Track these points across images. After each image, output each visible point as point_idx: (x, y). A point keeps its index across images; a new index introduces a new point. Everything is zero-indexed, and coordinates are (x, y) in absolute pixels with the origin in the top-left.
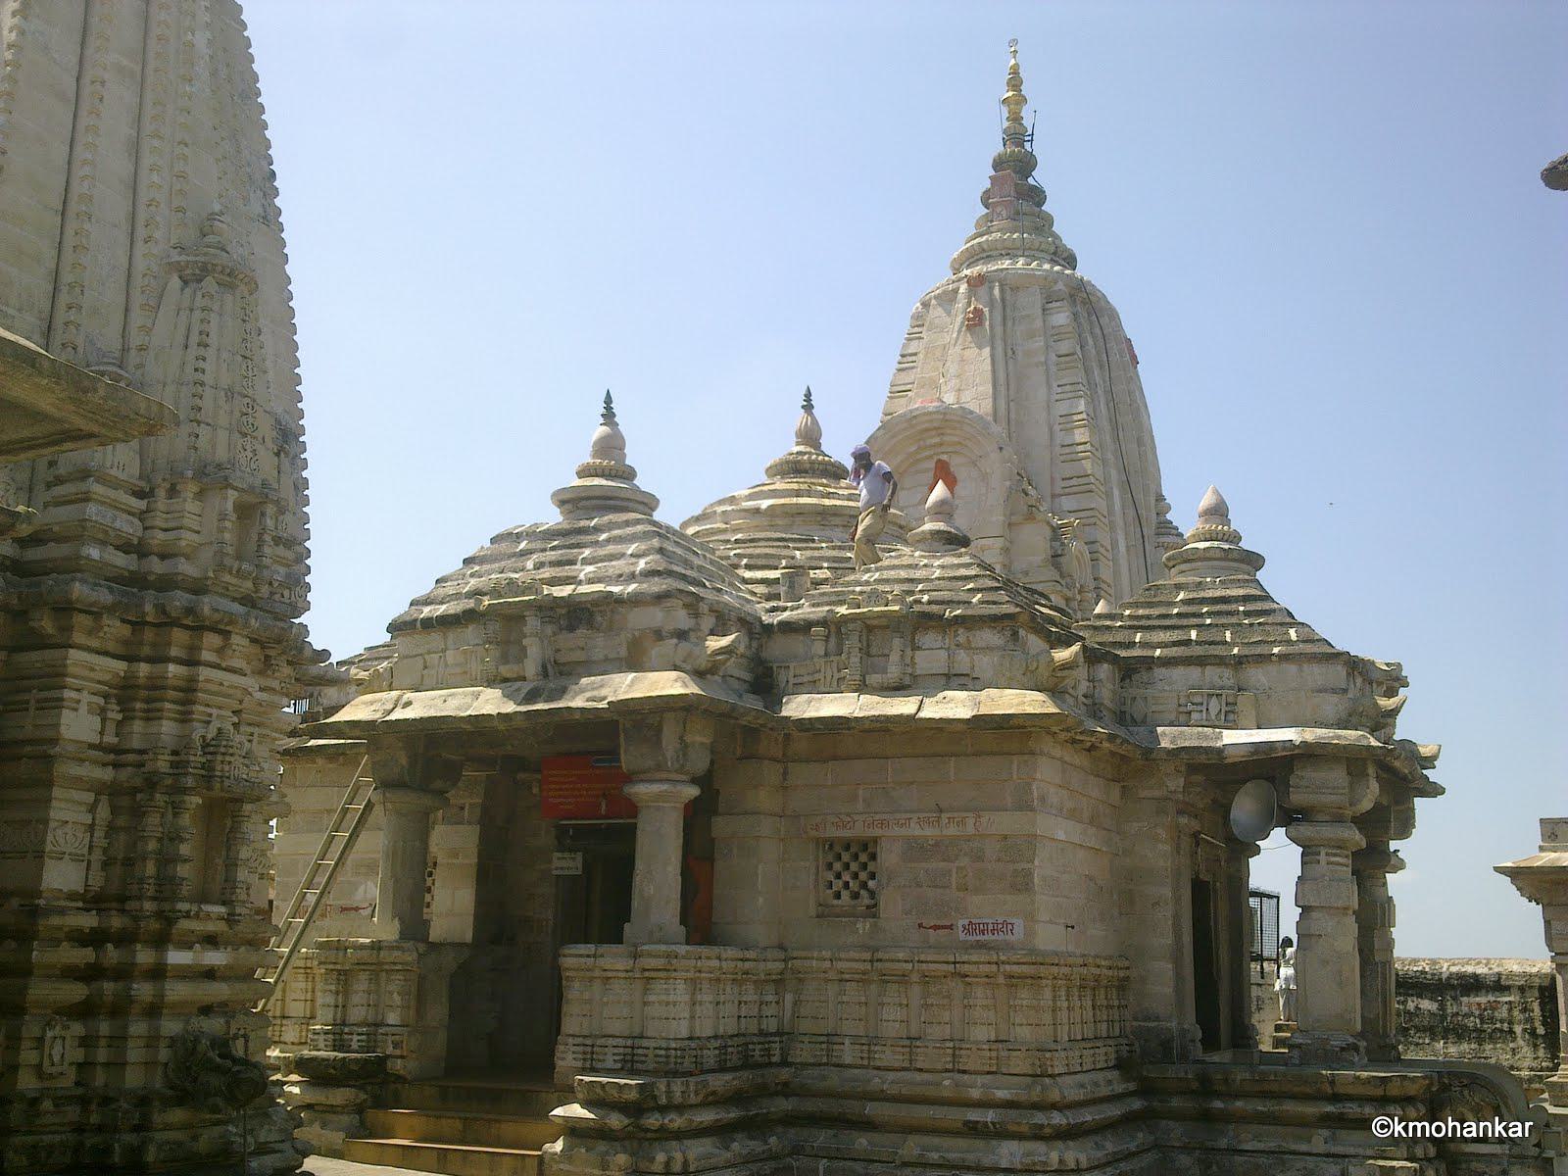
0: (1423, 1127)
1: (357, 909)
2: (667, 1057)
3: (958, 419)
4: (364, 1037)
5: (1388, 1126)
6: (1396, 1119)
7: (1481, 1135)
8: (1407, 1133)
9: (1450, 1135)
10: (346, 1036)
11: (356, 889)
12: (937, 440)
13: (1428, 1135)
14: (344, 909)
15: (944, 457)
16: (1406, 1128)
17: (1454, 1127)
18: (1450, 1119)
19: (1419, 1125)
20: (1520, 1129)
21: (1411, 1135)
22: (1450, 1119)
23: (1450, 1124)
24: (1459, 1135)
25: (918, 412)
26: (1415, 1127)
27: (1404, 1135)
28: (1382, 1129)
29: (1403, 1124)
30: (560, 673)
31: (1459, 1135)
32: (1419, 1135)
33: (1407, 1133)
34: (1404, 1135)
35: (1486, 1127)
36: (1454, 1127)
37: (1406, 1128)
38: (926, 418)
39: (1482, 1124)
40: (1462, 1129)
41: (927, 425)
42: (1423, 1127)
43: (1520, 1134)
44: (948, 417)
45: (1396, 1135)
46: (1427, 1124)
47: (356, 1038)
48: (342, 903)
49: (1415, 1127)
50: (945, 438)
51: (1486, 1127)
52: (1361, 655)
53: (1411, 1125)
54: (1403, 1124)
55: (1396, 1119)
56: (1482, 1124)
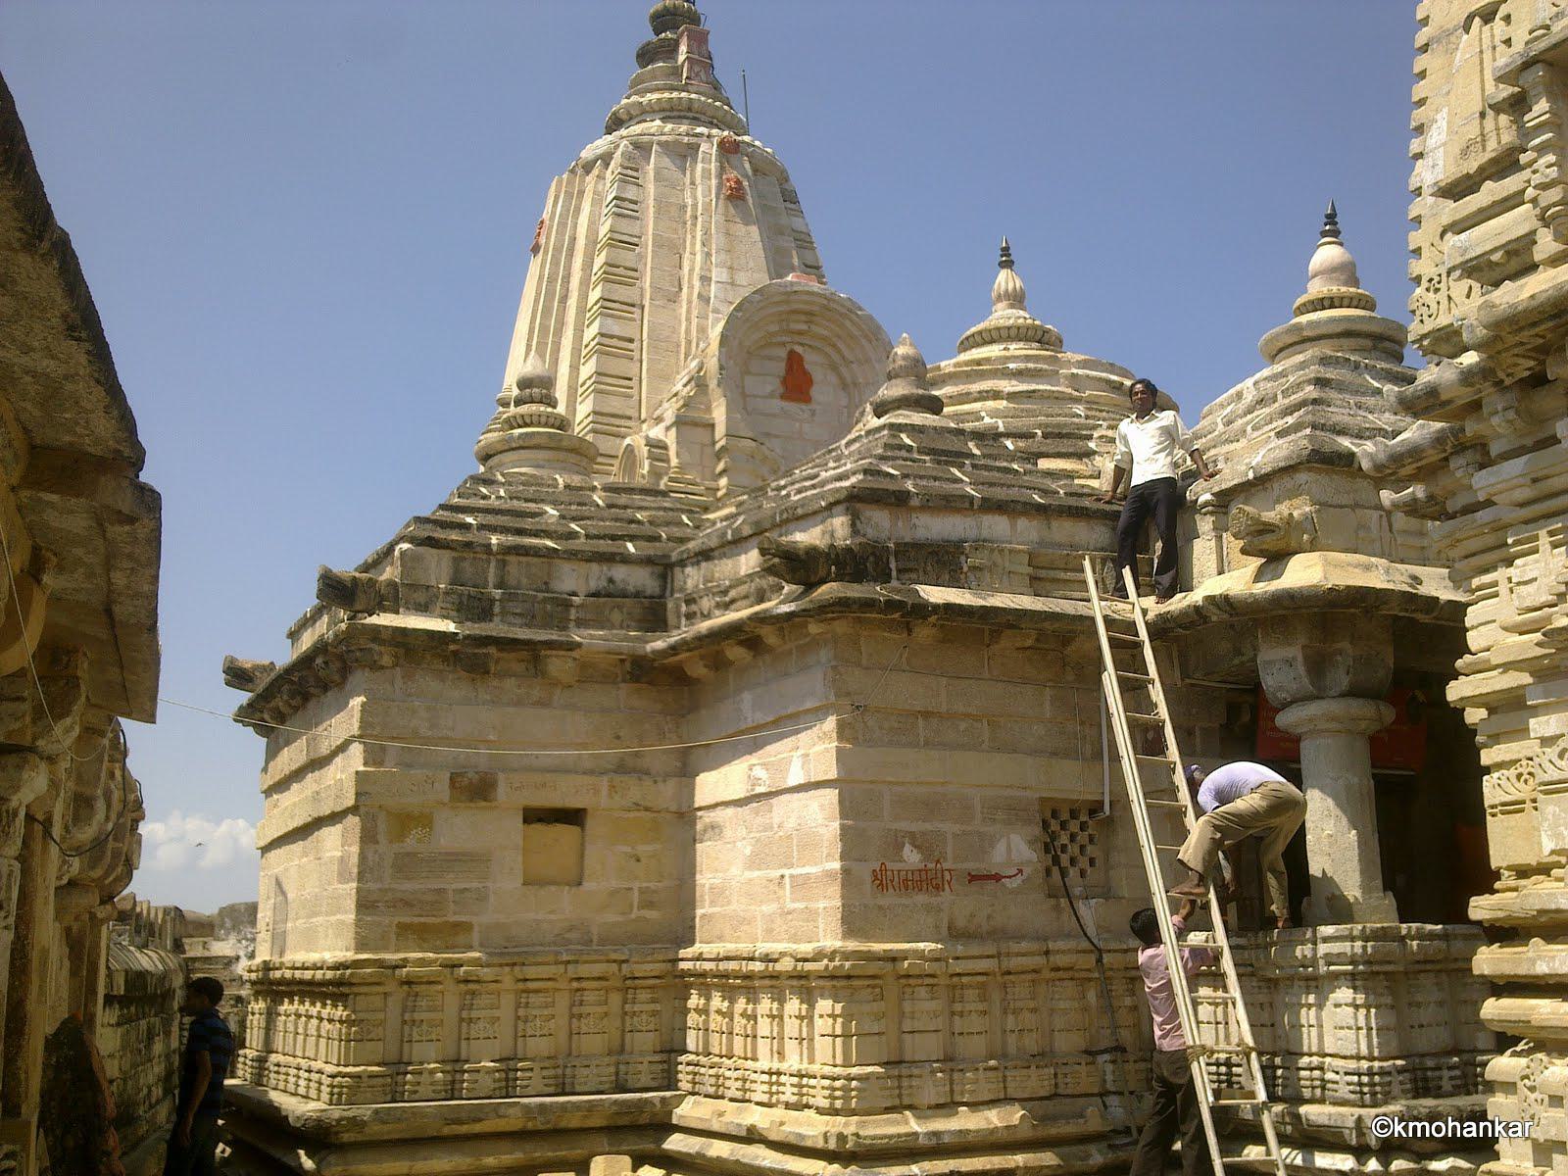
0: (1423, 1127)
1: (997, 878)
2: (1360, 1084)
3: (844, 311)
4: (1457, 1073)
5: (1389, 1126)
6: (1396, 1119)
7: (1481, 1135)
8: (1407, 1134)
9: (1450, 1135)
10: (1429, 1073)
11: (992, 845)
12: (804, 327)
13: (1428, 1135)
14: (973, 878)
15: (799, 349)
16: (1405, 1128)
17: (1454, 1127)
18: (1450, 1119)
19: (1419, 1125)
20: (1474, 1129)
21: (1411, 1135)
22: (1450, 1119)
23: (1450, 1124)
24: (1459, 1135)
25: (801, 289)
26: (1415, 1128)
27: (1404, 1135)
28: (1382, 1129)
29: (1403, 1124)
30: (1276, 561)
31: (1459, 1135)
32: (1419, 1135)
33: (1407, 1134)
34: (1404, 1135)
35: (1486, 1127)
36: (1454, 1127)
37: (1405, 1128)
38: (805, 297)
39: (1482, 1125)
40: (1462, 1129)
41: (801, 306)
42: (1423, 1127)
43: (1474, 1134)
44: (833, 305)
45: (1396, 1135)
46: (1427, 1125)
47: (1446, 1074)
48: (972, 866)
49: (1415, 1128)
50: (813, 327)
51: (1486, 1127)
52: (160, 632)
53: (1411, 1125)
54: (1403, 1124)
55: (1396, 1119)
56: (1482, 1125)
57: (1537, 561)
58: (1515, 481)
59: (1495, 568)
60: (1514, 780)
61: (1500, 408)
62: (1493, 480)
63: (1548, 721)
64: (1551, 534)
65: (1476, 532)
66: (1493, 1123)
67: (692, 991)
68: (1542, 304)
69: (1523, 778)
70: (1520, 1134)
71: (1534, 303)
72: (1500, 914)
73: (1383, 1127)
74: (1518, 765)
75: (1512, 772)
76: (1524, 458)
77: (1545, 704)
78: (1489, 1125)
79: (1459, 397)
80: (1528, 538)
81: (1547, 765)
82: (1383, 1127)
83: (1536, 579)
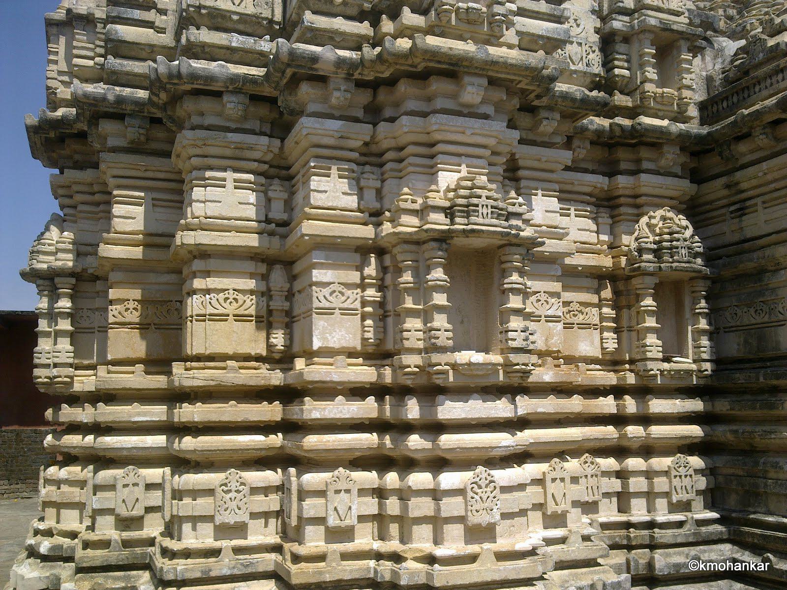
0: (714, 565)
16: (706, 566)
19: (712, 565)
20: (740, 566)
23: (728, 564)
26: (710, 565)
35: (746, 566)
37: (706, 566)
40: (734, 566)
42: (714, 565)
49: (710, 565)
51: (746, 566)
53: (708, 564)
56: (744, 564)
57: (328, 182)
58: (331, 132)
59: (225, 170)
60: (222, 301)
61: (342, 88)
62: (317, 126)
63: (326, 274)
64: (339, 170)
65: (224, 144)
66: (749, 563)
67: (372, 255)
68: (455, 56)
69: (229, 301)
70: (763, 569)
71: (451, 52)
72: (212, 383)
73: (694, 565)
74: (226, 292)
75: (221, 296)
76: (341, 123)
77: (322, 263)
78: (748, 564)
79: (323, 70)
80: (321, 166)
81: (321, 298)
82: (694, 565)
83: (326, 192)
